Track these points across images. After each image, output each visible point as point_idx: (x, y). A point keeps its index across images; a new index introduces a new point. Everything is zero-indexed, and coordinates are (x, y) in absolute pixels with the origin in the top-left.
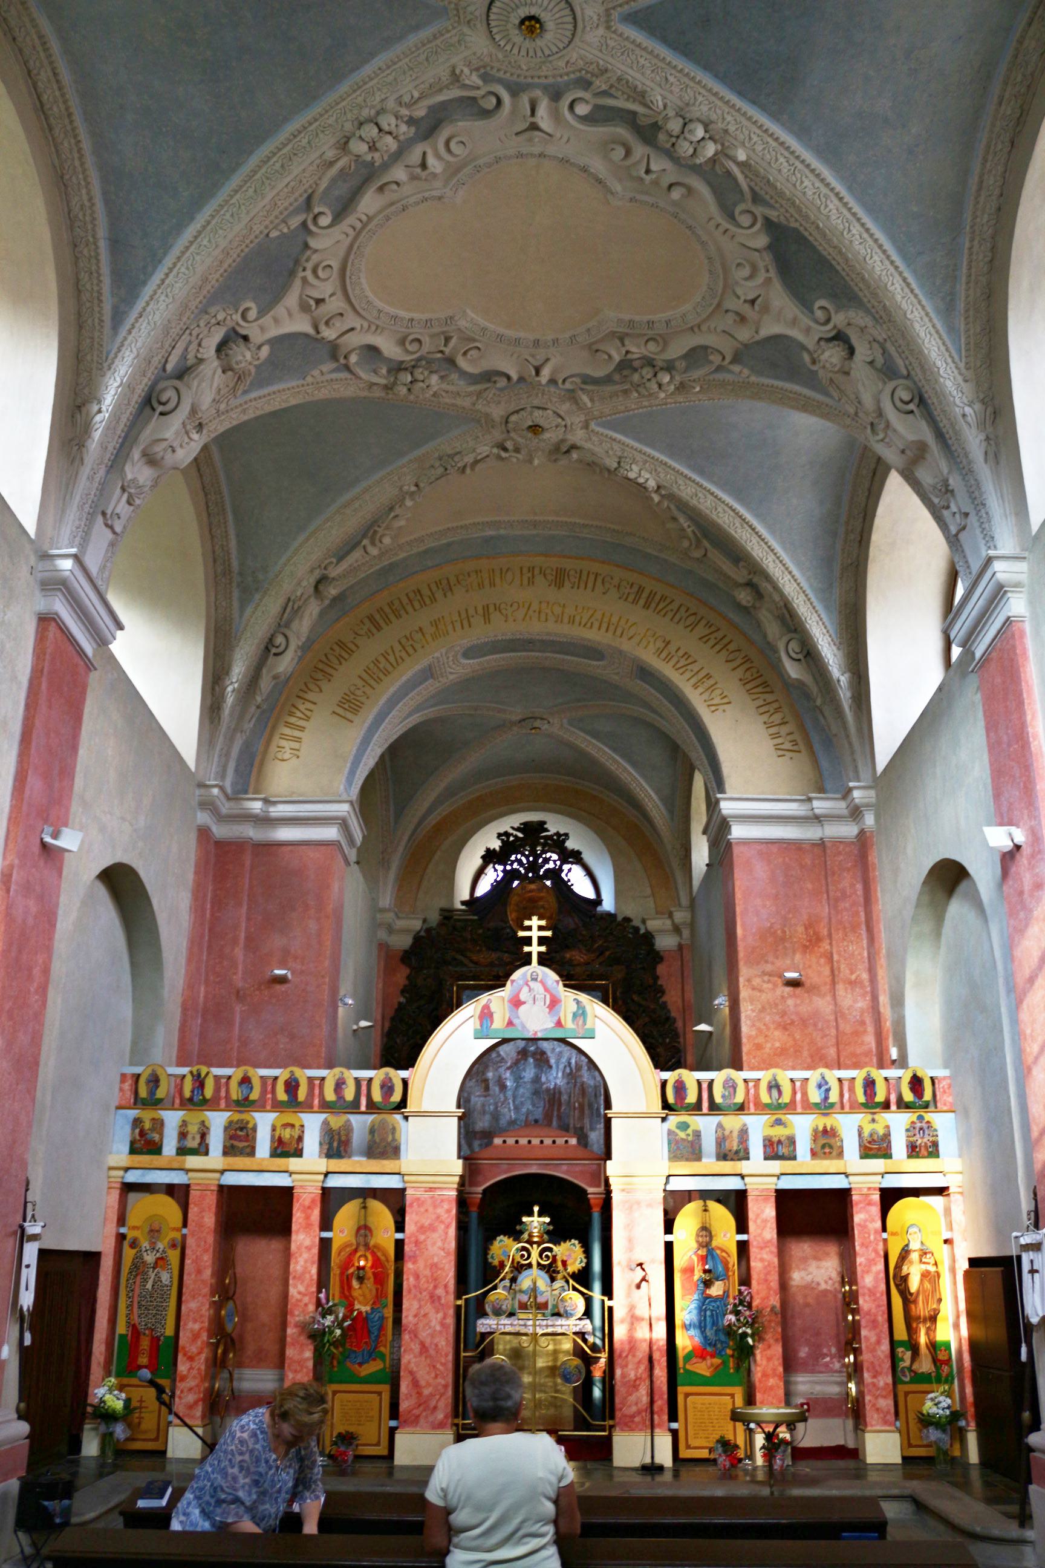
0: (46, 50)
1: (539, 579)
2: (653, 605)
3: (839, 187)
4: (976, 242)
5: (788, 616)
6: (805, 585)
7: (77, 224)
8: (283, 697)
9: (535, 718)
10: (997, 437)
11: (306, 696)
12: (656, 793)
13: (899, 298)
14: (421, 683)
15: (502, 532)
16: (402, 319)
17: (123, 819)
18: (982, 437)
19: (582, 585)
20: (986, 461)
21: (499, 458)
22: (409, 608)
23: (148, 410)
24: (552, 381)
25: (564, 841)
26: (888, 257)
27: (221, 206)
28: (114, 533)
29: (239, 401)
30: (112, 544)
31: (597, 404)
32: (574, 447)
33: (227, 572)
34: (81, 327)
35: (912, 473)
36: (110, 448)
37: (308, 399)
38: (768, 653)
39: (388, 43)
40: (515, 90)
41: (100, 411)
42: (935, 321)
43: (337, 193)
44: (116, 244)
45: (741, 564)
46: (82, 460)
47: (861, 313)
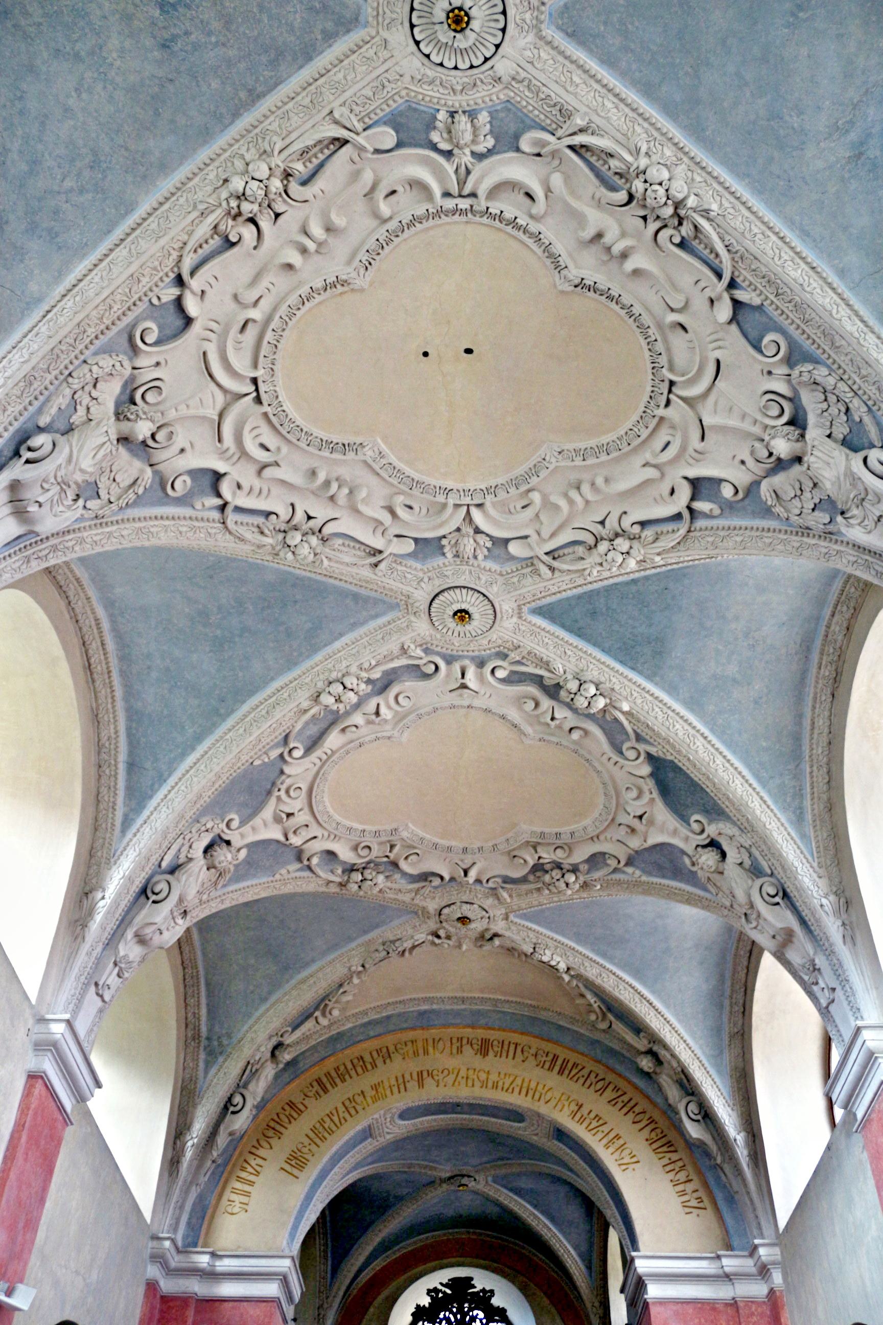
0: (99, 628)
1: (467, 1050)
2: (566, 1072)
3: (703, 729)
4: (815, 768)
5: (685, 1081)
6: (699, 1053)
7: (104, 750)
8: (237, 1153)
9: (463, 1176)
10: (851, 923)
11: (257, 1152)
12: (575, 1249)
13: (758, 812)
14: (360, 1143)
15: (435, 1007)
16: (356, 830)
17: (77, 1273)
18: (839, 923)
19: (504, 1054)
20: (844, 943)
21: (433, 943)
22: (353, 1073)
23: (143, 898)
24: (478, 881)
25: (490, 1298)
26: (747, 781)
27: (217, 741)
28: (103, 1001)
29: (219, 893)
30: (101, 1011)
31: (515, 899)
32: (496, 935)
33: (197, 1037)
34: (96, 829)
35: (783, 954)
36: (108, 929)
37: (276, 892)
38: (670, 1111)
39: (354, 626)
40: (449, 660)
41: (103, 898)
42: (790, 830)
43: (308, 733)
44: (131, 766)
45: (642, 1034)
46: (84, 938)
47: (729, 825)
